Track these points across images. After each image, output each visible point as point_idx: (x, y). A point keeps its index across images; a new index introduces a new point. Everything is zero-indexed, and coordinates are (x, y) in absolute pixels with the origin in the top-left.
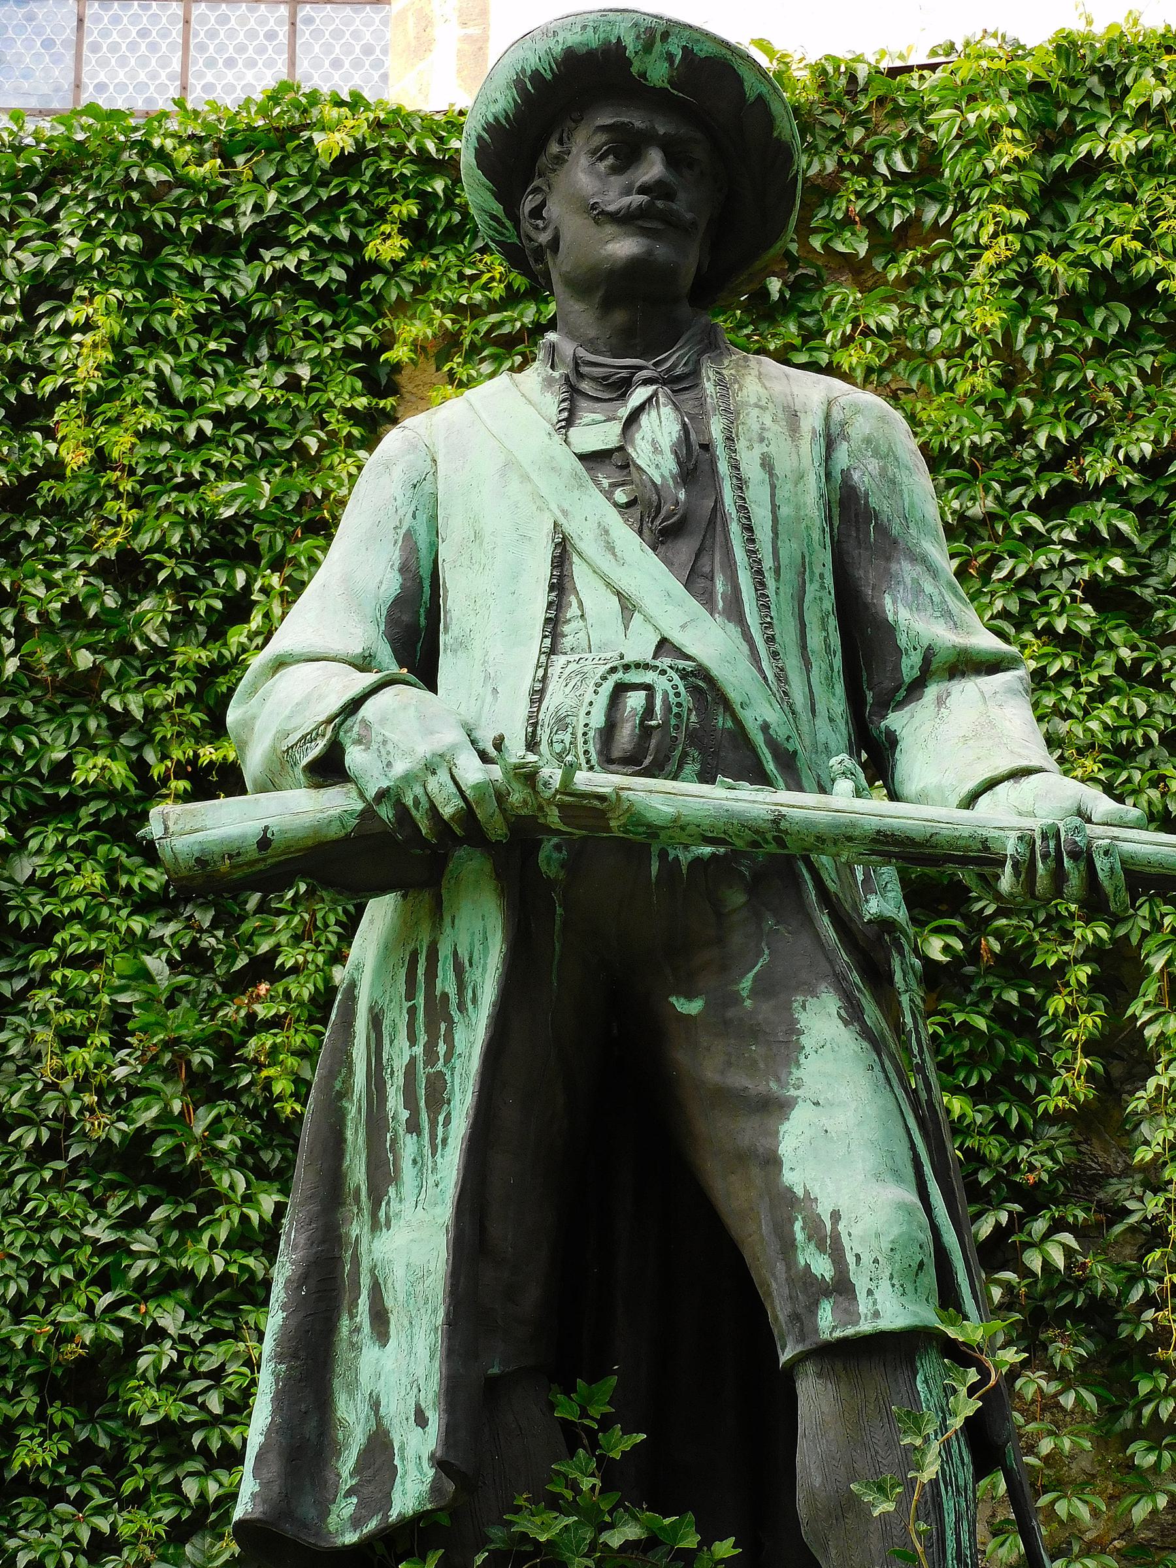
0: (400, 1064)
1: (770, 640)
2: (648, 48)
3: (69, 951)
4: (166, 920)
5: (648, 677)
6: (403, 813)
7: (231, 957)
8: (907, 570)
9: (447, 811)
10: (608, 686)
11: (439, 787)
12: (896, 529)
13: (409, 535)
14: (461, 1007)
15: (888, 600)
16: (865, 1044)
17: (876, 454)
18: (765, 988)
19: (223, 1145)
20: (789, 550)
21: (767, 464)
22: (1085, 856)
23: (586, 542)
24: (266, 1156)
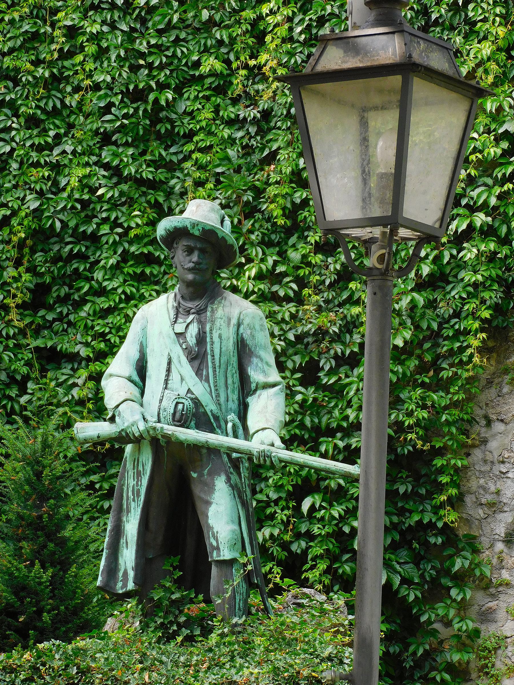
0: (131, 485)
1: (216, 386)
2: (193, 228)
3: (199, 145)
4: (239, 129)
5: (183, 401)
6: (127, 434)
7: (262, 150)
8: (255, 360)
9: (136, 435)
10: (175, 403)
11: (135, 430)
12: (253, 349)
13: (141, 343)
14: (143, 474)
15: (249, 369)
16: (230, 488)
17: (250, 329)
18: (210, 474)
19: (253, 237)
20: (224, 359)
21: (220, 337)
22: (270, 457)
23: (175, 361)
24: (273, 237)
